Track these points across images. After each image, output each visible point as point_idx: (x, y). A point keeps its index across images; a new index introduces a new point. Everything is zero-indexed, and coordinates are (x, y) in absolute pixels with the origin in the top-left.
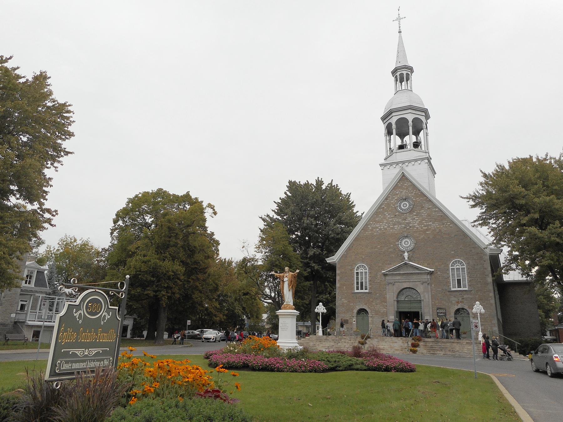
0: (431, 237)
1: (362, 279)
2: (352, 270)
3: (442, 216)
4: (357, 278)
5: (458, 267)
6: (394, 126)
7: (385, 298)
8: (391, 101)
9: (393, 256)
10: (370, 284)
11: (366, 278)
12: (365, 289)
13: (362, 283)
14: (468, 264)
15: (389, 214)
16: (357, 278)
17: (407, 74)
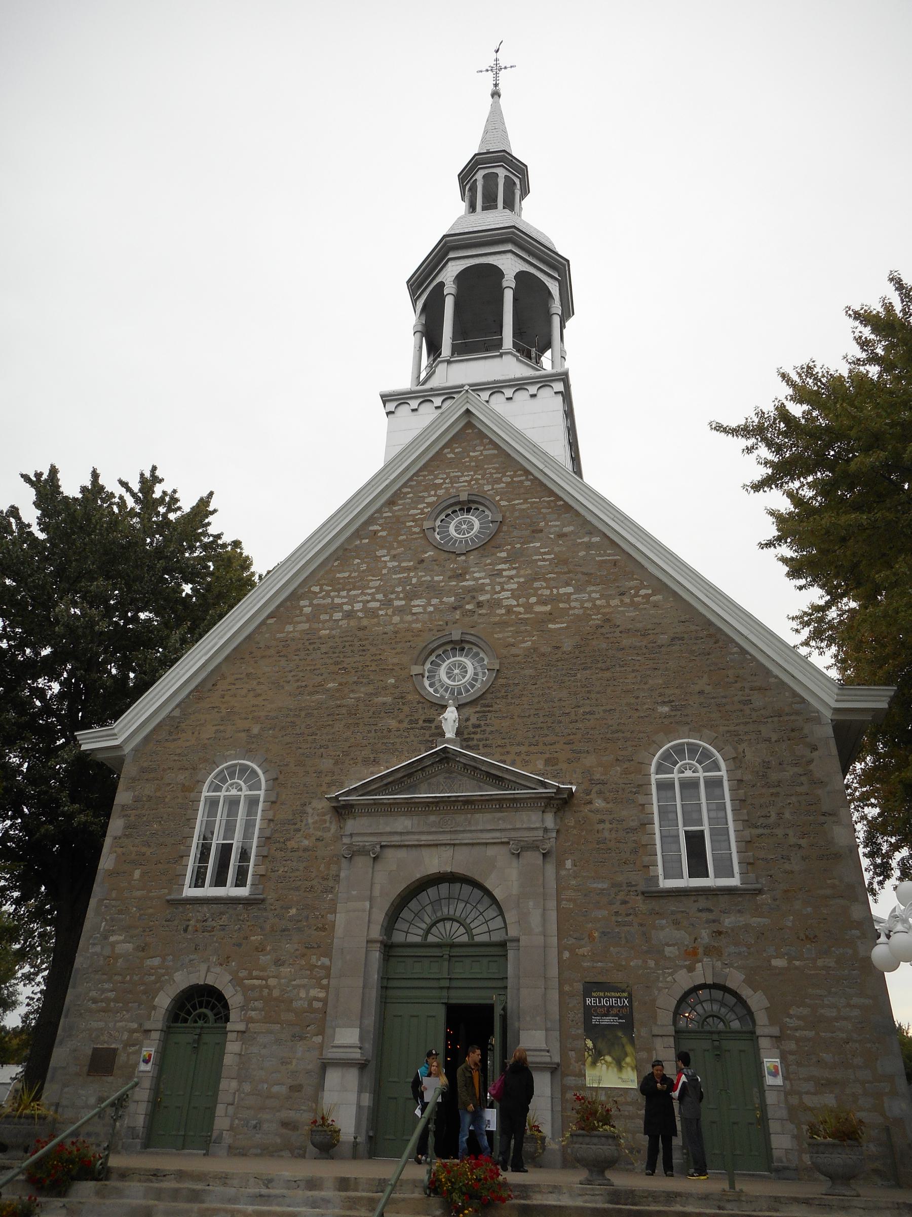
0: (568, 645)
2: (191, 788)
3: (615, 559)
4: (666, 813)
7: (327, 928)
9: (393, 724)
13: (225, 850)
14: (736, 762)
16: (666, 813)
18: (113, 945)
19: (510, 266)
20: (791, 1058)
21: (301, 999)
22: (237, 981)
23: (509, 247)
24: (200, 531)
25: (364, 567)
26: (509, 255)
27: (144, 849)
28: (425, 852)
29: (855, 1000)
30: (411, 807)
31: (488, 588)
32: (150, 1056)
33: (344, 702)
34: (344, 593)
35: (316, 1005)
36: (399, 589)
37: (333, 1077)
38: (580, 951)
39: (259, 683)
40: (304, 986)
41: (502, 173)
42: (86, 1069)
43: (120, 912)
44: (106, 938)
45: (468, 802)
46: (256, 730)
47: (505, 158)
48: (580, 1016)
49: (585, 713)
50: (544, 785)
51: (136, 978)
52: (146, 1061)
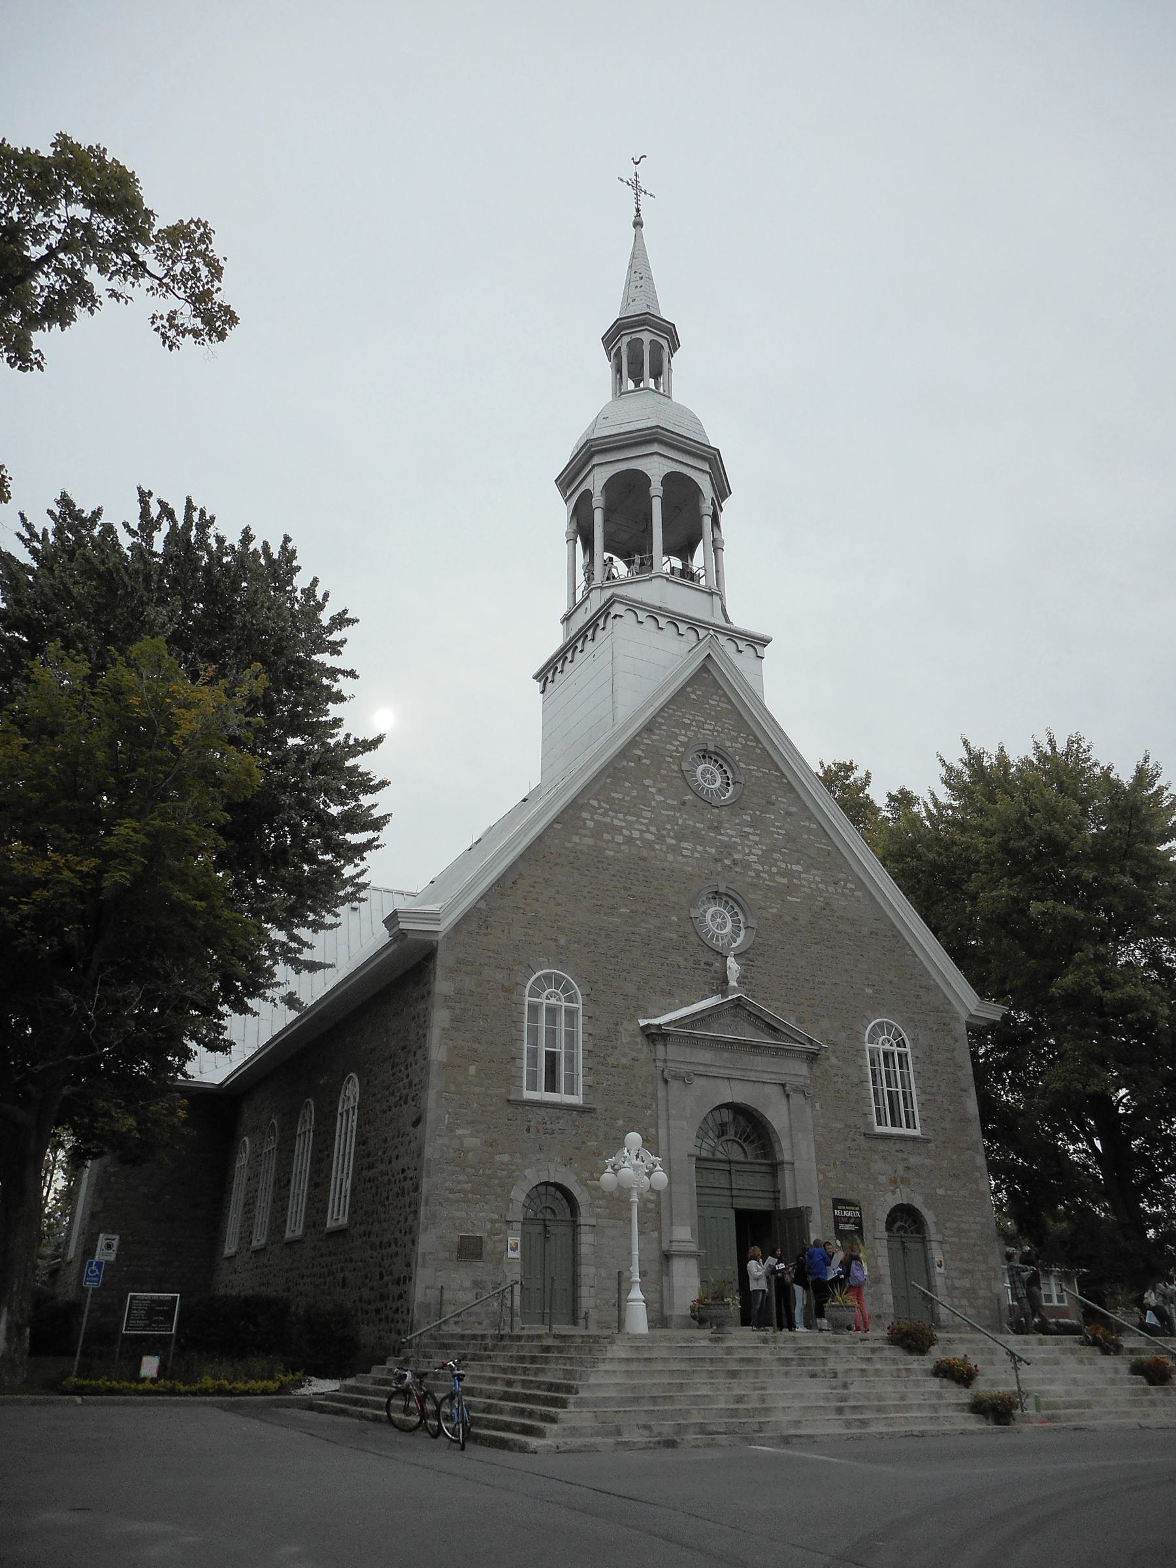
1: (552, 1035)
2: (512, 989)
6: (598, 500)
8: (603, 417)
9: (681, 961)
10: (589, 1069)
11: (571, 1036)
12: (893, 1125)
13: (552, 1058)
15: (660, 791)
17: (656, 348)
18: (460, 1137)
20: (948, 1255)
24: (928, 823)
25: (634, 793)
26: (656, 458)
27: (475, 1046)
28: (720, 1082)
29: (978, 1219)
30: (716, 1044)
31: (739, 848)
33: (637, 930)
34: (621, 816)
35: (651, 1206)
36: (669, 827)
37: (678, 1266)
38: (830, 1175)
39: (558, 892)
41: (646, 337)
42: (455, 1255)
44: (452, 1131)
45: (756, 1047)
46: (562, 942)
48: (832, 1225)
49: (819, 983)
50: (811, 1041)
51: (488, 1172)
52: (514, 1250)
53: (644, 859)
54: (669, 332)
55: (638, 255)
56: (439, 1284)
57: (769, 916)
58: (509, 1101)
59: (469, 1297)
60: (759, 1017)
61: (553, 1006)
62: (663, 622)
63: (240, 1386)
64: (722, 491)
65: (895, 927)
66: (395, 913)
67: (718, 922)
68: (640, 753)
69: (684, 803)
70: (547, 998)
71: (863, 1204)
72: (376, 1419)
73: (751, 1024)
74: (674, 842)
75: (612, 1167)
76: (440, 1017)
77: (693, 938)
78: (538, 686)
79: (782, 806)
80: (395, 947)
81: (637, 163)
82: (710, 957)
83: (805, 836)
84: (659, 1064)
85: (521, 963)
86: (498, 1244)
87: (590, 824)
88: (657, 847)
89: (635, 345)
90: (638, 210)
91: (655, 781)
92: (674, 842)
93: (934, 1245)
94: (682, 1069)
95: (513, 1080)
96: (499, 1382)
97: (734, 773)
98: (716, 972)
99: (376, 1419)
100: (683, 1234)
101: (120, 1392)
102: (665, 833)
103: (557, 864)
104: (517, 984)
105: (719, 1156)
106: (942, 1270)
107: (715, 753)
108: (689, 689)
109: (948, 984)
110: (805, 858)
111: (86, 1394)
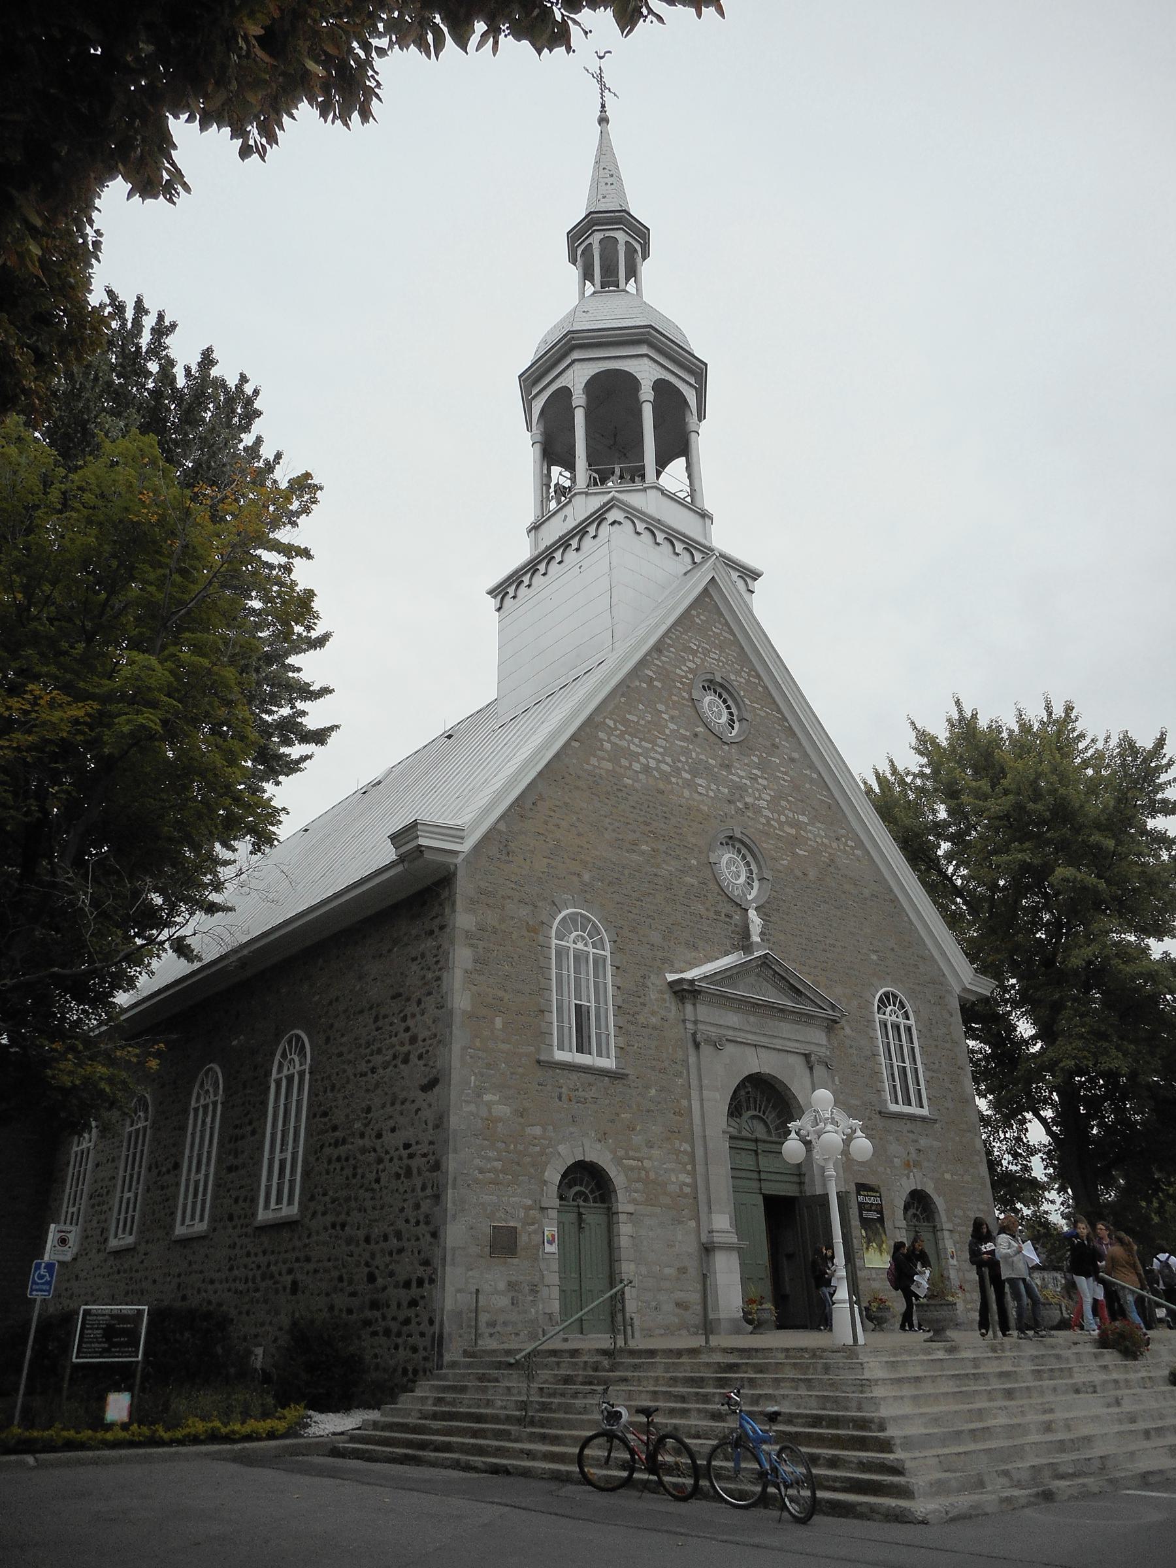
2: (538, 928)
5: (580, 946)
6: (579, 398)
17: (630, 252)
18: (489, 1105)
19: (646, 372)
21: (673, 1183)
22: (618, 1161)
23: (644, 350)
26: (646, 360)
27: (501, 993)
32: (553, 1236)
34: (636, 741)
35: (687, 1190)
40: (673, 1170)
41: (621, 237)
43: (489, 1066)
44: (479, 1096)
46: (586, 877)
47: (622, 219)
49: (830, 945)
50: (833, 1007)
51: (520, 1147)
52: (551, 1242)
53: (662, 792)
54: (641, 233)
55: (604, 150)
56: (470, 1288)
57: (781, 868)
58: (539, 1062)
59: (504, 1301)
60: (784, 978)
61: (579, 955)
62: (660, 537)
63: (252, 1425)
64: (701, 416)
65: (891, 891)
66: (414, 825)
67: (732, 870)
68: (651, 674)
69: (696, 735)
70: (575, 943)
71: (882, 1189)
72: (562, 1478)
73: (776, 987)
74: (688, 776)
75: (797, 1133)
76: (462, 957)
77: (713, 886)
78: (492, 603)
79: (786, 751)
80: (400, 868)
81: (601, 58)
82: (729, 908)
83: (808, 786)
84: (689, 1025)
85: (545, 899)
86: (533, 1236)
87: (607, 746)
88: (674, 780)
89: (609, 244)
90: (603, 106)
91: (667, 706)
92: (688, 776)
93: (946, 1234)
94: (713, 1032)
95: (543, 1035)
96: (694, 1414)
97: (739, 708)
98: (736, 925)
99: (562, 1478)
100: (722, 1222)
101: (82, 1446)
102: (680, 765)
103: (577, 788)
104: (543, 923)
105: (745, 1134)
106: (954, 1262)
107: (721, 686)
108: (694, 612)
109: (943, 954)
110: (809, 808)
111: (40, 1452)
